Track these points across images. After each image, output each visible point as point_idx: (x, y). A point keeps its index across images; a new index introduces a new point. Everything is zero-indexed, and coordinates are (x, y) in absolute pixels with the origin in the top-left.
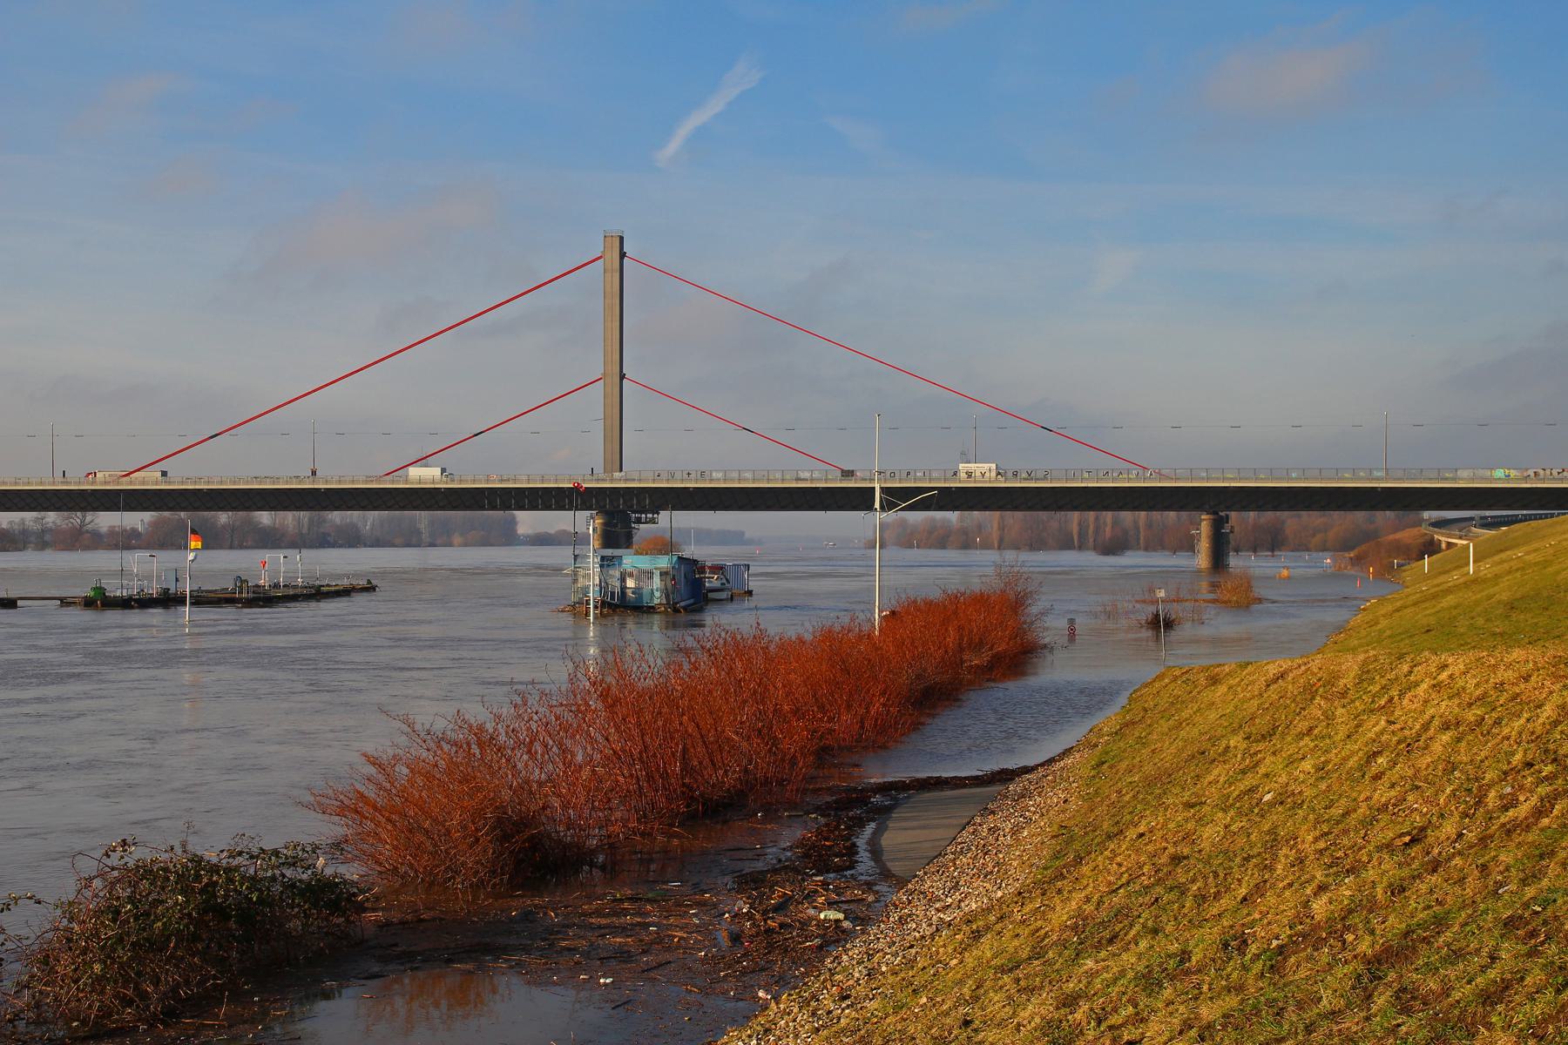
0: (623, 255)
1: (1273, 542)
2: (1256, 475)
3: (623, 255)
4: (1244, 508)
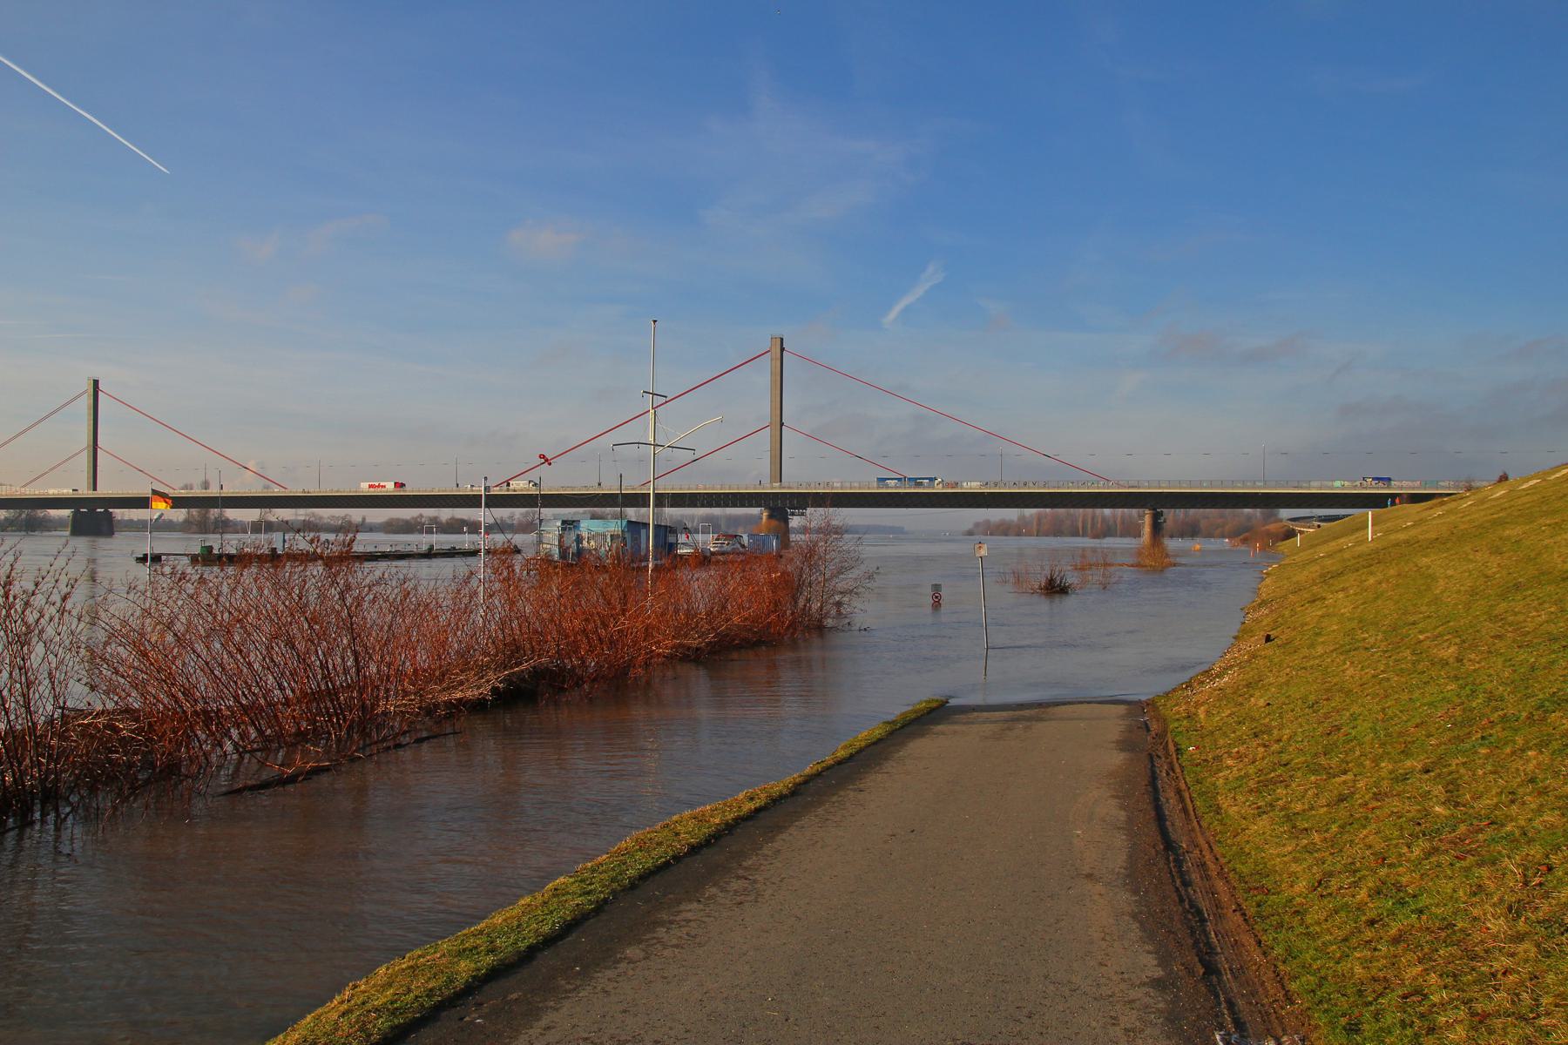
0: (782, 349)
1: (1192, 531)
2: (1190, 485)
3: (782, 349)
4: (1173, 507)
